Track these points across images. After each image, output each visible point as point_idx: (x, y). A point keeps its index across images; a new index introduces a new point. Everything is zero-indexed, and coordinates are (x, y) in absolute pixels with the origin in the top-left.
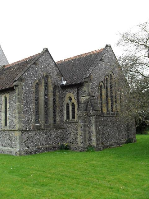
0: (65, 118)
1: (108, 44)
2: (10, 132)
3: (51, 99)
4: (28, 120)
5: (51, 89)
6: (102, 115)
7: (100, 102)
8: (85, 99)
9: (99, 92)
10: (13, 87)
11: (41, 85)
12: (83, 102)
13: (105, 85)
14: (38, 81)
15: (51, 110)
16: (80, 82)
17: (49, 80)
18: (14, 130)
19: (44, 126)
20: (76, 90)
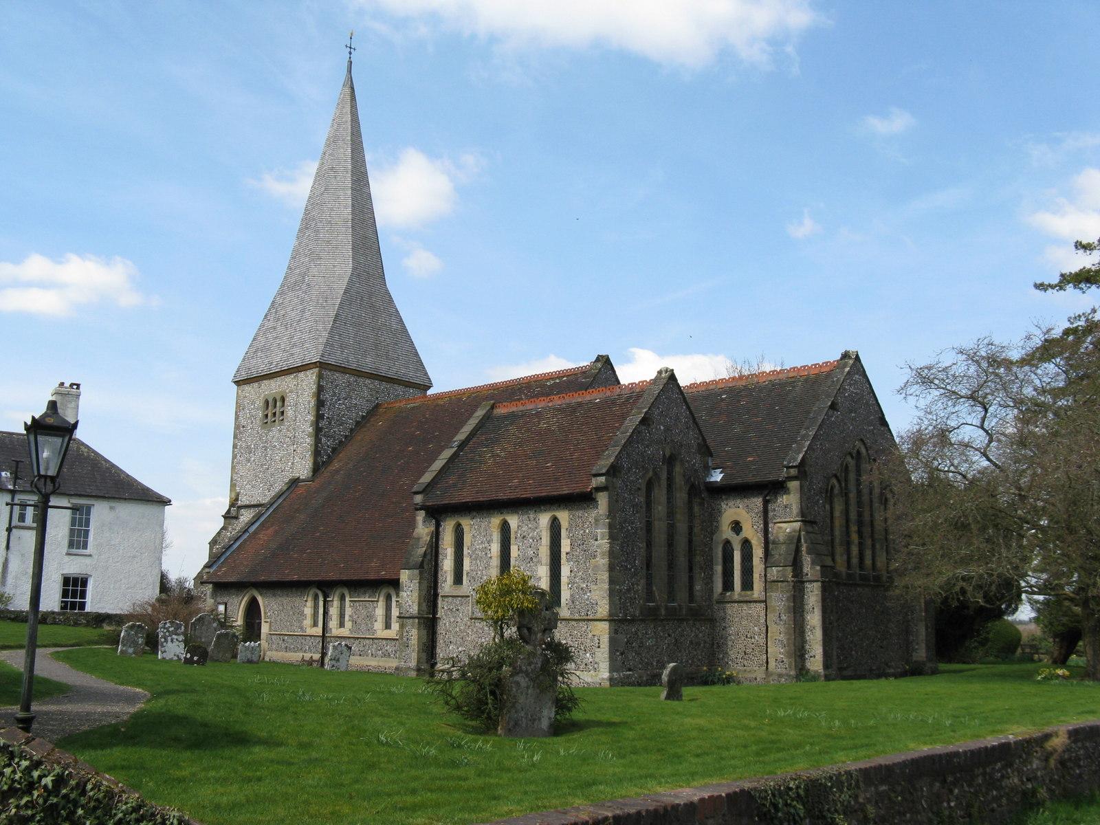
1: (848, 350)
2: (574, 623)
3: (682, 527)
4: (629, 590)
5: (681, 496)
7: (830, 538)
9: (828, 507)
10: (591, 492)
11: (660, 486)
12: (781, 539)
13: (843, 485)
14: (651, 474)
15: (682, 561)
16: (772, 478)
17: (678, 469)
18: (591, 617)
19: (667, 608)
20: (758, 502)
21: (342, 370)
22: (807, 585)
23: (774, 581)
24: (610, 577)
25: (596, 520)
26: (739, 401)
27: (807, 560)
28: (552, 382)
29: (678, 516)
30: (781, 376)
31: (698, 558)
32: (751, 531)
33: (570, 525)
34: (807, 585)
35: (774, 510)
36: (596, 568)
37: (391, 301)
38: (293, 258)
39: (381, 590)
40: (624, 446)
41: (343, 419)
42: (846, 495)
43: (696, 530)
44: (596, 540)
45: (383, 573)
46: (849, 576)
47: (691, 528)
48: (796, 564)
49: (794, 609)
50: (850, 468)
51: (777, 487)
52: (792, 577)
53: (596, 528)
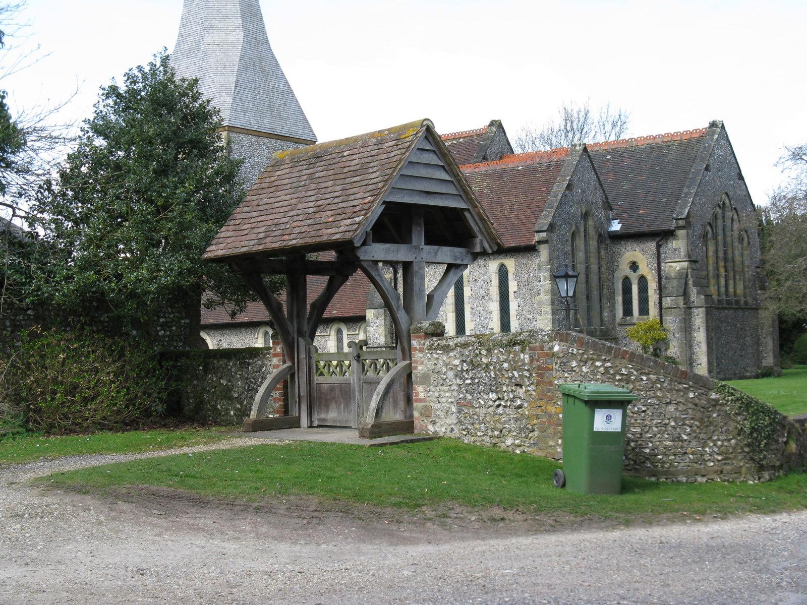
0: (620, 312)
1: (715, 119)
3: (594, 267)
5: (593, 243)
6: (721, 306)
7: (706, 273)
8: (678, 268)
9: (704, 248)
11: (580, 237)
12: (673, 275)
14: (574, 227)
15: (595, 293)
17: (591, 222)
20: (652, 246)
21: (246, 131)
22: (695, 310)
23: (668, 308)
24: (553, 309)
25: (539, 266)
26: (623, 162)
27: (693, 291)
28: (450, 143)
29: (592, 260)
30: (656, 141)
31: (605, 291)
32: (646, 268)
33: (517, 270)
34: (695, 310)
35: (666, 252)
36: (540, 303)
37: (277, 65)
38: (183, 25)
39: (361, 325)
40: (557, 208)
41: (250, 176)
42: (715, 236)
43: (603, 270)
44: (540, 281)
45: (335, 312)
46: (719, 301)
47: (599, 268)
48: (685, 294)
49: (685, 329)
50: (718, 216)
51: (668, 234)
52: (684, 304)
53: (539, 272)
